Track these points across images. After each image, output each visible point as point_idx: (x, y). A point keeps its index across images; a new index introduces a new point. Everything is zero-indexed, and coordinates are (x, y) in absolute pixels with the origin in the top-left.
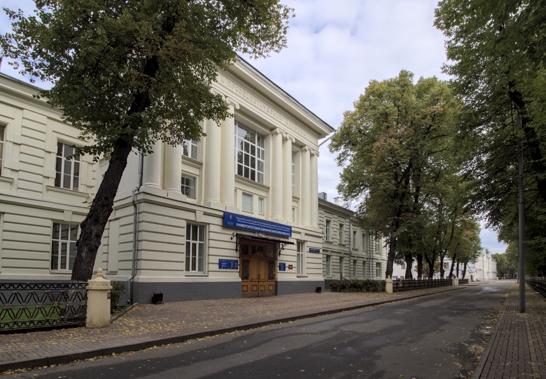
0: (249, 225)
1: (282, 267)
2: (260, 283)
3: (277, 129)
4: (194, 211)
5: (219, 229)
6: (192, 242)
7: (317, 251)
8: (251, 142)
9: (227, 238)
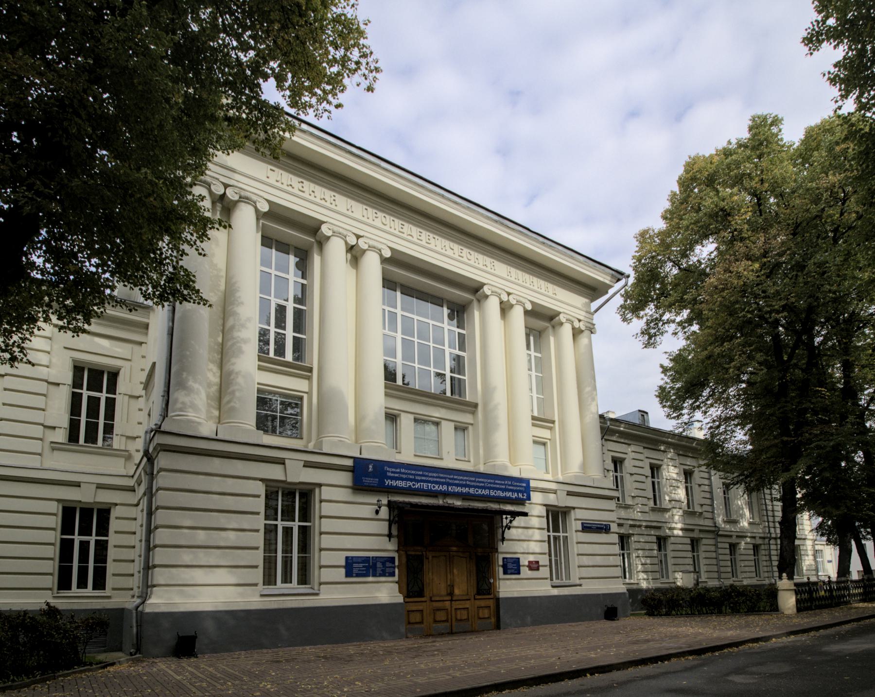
0: (418, 481)
1: (510, 566)
2: (456, 605)
3: (561, 316)
4: (281, 462)
5: (344, 494)
6: (281, 524)
7: (604, 529)
8: (432, 319)
9: (367, 511)
